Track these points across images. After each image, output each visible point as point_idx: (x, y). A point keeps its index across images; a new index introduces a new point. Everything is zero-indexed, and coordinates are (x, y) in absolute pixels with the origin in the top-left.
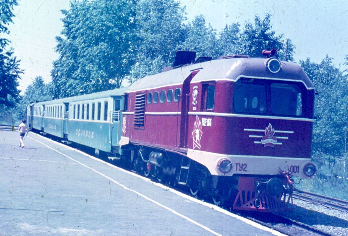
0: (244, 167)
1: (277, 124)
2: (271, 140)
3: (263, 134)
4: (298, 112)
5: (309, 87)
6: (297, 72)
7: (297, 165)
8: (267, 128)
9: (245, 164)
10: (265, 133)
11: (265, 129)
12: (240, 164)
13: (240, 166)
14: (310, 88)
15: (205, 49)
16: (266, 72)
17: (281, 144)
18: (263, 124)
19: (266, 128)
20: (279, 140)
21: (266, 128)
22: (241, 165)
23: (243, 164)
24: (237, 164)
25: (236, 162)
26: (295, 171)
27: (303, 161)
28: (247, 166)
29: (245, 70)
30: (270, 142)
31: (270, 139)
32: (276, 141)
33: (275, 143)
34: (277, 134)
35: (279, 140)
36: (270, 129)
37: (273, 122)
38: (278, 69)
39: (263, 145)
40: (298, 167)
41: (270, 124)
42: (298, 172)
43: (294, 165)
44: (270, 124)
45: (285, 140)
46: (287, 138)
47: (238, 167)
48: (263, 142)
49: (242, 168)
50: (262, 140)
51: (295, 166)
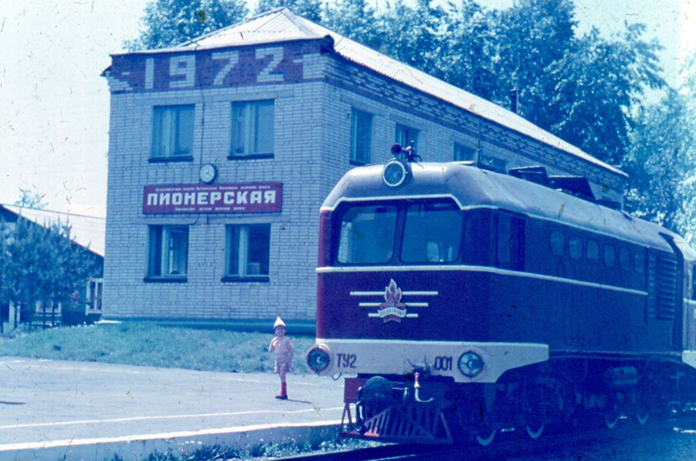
0: (351, 360)
1: (406, 281)
2: (394, 308)
3: (380, 299)
4: (505, 255)
5: (464, 204)
6: (441, 180)
7: (448, 356)
8: (388, 288)
9: (354, 356)
10: (385, 297)
11: (383, 290)
12: (344, 355)
13: (344, 358)
14: (468, 208)
15: (86, 270)
16: (381, 188)
17: (416, 315)
18: (378, 281)
19: (386, 288)
20: (410, 310)
21: (386, 288)
22: (346, 357)
23: (350, 355)
24: (340, 355)
25: (339, 352)
26: (445, 366)
27: (459, 347)
28: (358, 359)
29: (348, 188)
30: (392, 313)
31: (391, 308)
32: (405, 311)
33: (403, 314)
34: (405, 299)
35: (410, 310)
36: (392, 289)
37: (396, 275)
38: (398, 181)
39: (382, 319)
40: (450, 360)
41: (392, 281)
42: (451, 369)
43: (442, 356)
44: (392, 281)
45: (423, 308)
46: (426, 304)
47: (342, 361)
48: (381, 314)
49: (348, 361)
50: (379, 311)
51: (445, 357)
